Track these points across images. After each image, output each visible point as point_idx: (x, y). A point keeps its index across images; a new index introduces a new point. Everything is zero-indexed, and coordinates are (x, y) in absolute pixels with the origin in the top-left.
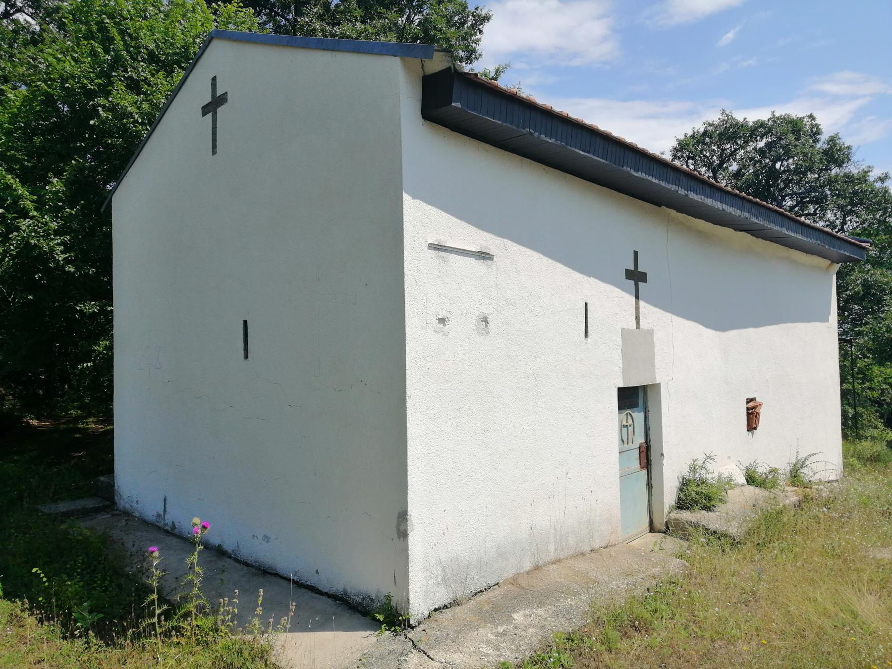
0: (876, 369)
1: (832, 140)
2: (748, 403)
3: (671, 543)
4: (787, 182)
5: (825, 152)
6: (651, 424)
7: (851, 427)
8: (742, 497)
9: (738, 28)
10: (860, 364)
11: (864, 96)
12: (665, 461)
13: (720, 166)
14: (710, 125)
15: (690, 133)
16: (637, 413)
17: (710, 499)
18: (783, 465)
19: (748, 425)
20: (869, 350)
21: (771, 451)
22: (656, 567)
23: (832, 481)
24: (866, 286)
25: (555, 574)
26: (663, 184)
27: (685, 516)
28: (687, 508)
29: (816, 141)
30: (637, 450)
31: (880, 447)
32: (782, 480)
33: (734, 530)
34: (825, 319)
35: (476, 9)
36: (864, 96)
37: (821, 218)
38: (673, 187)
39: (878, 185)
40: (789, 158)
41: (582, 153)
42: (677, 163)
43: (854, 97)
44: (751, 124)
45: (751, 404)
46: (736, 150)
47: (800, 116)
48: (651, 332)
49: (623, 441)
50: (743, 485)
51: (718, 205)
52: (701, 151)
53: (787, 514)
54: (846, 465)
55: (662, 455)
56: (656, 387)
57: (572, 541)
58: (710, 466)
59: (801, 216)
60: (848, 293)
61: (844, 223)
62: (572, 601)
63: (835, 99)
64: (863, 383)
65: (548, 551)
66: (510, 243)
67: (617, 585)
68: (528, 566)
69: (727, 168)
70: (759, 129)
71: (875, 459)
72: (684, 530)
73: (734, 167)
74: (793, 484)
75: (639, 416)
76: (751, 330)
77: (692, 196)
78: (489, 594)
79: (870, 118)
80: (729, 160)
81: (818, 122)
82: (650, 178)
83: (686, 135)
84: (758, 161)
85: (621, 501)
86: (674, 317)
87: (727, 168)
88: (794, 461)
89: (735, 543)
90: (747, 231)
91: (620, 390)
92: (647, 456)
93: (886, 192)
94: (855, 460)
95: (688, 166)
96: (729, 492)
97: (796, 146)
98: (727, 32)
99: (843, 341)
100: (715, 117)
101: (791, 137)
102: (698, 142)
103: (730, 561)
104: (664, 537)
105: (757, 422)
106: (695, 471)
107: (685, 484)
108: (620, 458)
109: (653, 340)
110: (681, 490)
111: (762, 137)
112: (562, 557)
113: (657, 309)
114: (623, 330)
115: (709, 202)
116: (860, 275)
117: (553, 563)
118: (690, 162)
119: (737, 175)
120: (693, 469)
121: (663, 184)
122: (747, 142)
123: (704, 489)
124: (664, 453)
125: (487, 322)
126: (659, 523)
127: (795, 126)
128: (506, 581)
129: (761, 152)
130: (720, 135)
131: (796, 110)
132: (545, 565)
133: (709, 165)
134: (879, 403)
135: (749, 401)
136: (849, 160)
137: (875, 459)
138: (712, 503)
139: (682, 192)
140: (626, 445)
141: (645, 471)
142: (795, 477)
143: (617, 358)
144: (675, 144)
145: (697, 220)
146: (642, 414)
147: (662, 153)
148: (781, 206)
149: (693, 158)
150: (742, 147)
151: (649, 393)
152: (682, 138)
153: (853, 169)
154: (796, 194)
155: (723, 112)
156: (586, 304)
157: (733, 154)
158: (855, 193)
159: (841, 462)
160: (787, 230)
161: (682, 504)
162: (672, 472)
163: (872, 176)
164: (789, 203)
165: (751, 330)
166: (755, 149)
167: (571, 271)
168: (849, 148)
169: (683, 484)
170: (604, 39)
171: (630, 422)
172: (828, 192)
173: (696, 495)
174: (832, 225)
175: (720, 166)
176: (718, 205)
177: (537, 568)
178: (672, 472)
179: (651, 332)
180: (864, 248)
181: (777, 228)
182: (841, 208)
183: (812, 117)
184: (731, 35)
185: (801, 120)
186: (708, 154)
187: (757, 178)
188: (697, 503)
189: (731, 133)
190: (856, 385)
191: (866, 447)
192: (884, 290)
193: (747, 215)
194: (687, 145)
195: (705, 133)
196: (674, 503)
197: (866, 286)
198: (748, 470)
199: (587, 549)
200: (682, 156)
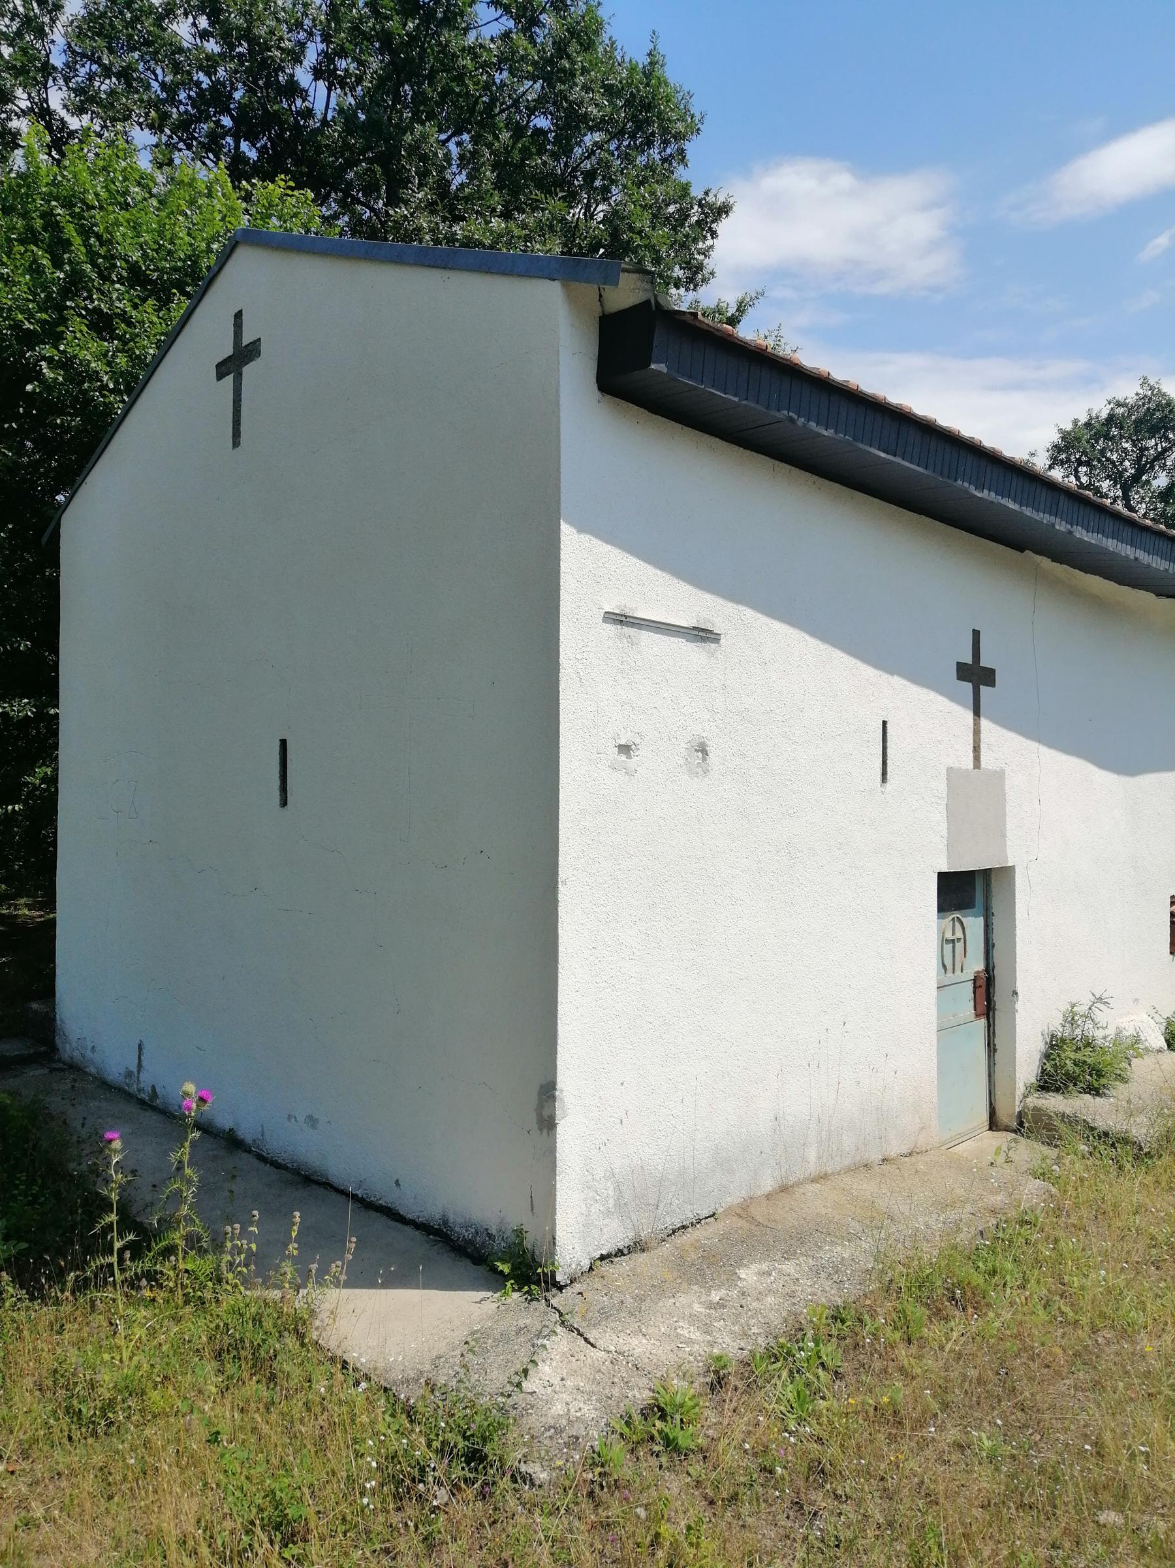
3: (1028, 1151)
6: (997, 938)
12: (1019, 1005)
13: (1136, 478)
14: (1119, 404)
15: (1083, 419)
22: (997, 1193)
25: (816, 1202)
26: (1028, 512)
27: (1054, 1103)
28: (1057, 1090)
30: (970, 985)
33: (1140, 1130)
35: (706, 193)
38: (1046, 518)
41: (883, 455)
42: (1057, 474)
49: (944, 966)
50: (1160, 1051)
51: (1127, 551)
55: (1015, 993)
58: (1099, 1016)
66: (749, 614)
68: (768, 1184)
69: (1148, 482)
72: (1050, 1128)
75: (974, 924)
77: (1080, 533)
78: (698, 1233)
80: (1152, 467)
82: (1004, 501)
83: (1075, 422)
86: (1043, 749)
87: (1148, 482)
89: (1141, 1155)
91: (942, 876)
92: (988, 995)
96: (1134, 1061)
100: (1129, 391)
106: (1073, 1022)
107: (1055, 1046)
108: (938, 998)
110: (1047, 1056)
112: (829, 1171)
114: (950, 770)
115: (1111, 544)
117: (814, 1181)
120: (1071, 1019)
124: (1019, 990)
126: (1004, 1116)
128: (729, 1211)
130: (1138, 422)
132: (799, 1184)
138: (1103, 1081)
139: (1061, 526)
140: (950, 974)
141: (983, 1022)
143: (938, 819)
144: (1056, 438)
151: (994, 884)
161: (1047, 1083)
167: (859, 663)
169: (1052, 1047)
171: (959, 934)
173: (1075, 1066)
175: (1136, 478)
176: (1127, 551)
177: (784, 1189)
179: (1000, 776)
186: (1114, 457)
194: (1078, 439)
199: (875, 1157)
200: (1068, 460)
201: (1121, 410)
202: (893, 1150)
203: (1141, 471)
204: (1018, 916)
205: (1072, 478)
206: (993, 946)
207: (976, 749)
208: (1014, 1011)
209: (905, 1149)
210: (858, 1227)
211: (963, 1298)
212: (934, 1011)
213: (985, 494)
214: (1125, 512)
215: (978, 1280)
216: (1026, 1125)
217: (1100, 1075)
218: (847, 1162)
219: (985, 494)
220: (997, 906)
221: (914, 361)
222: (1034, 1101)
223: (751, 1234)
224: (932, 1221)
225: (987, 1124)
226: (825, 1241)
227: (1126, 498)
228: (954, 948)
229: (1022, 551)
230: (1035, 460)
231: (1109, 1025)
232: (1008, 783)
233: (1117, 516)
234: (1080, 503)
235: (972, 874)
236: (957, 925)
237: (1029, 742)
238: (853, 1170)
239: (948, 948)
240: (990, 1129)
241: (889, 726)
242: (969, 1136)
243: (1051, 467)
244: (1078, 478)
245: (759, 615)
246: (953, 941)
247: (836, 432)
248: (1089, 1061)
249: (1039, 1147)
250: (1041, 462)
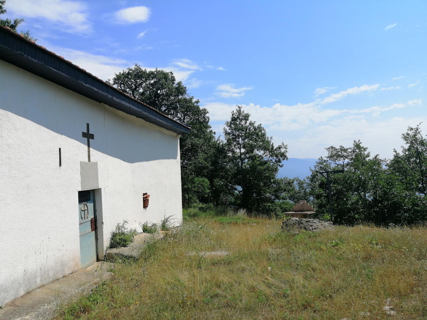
0: (196, 179)
1: (179, 84)
2: (143, 195)
3: (106, 265)
4: (163, 100)
5: (177, 88)
6: (97, 208)
7: (186, 203)
8: (141, 238)
9: (145, 32)
10: (191, 177)
11: (192, 70)
12: (104, 226)
13: (135, 89)
14: (130, 70)
15: (122, 73)
16: (89, 204)
17: (125, 241)
18: (159, 222)
19: (144, 205)
20: (193, 171)
21: (153, 216)
22: (97, 278)
23: (178, 226)
24: (192, 145)
25: (39, 294)
26: (100, 92)
27: (114, 251)
28: (115, 247)
29: (173, 83)
30: (90, 222)
31: (196, 210)
32: (159, 229)
33: (135, 253)
34: (175, 158)
36: (192, 70)
37: (176, 116)
38: (105, 94)
39: (196, 104)
40: (163, 89)
41: (55, 70)
42: (115, 86)
43: (189, 70)
44: (148, 72)
45: (145, 196)
46: (142, 83)
47: (167, 72)
48: (96, 164)
49: (82, 218)
50: (141, 233)
51: (128, 105)
52: (127, 82)
53: (160, 243)
54: (184, 219)
55: (103, 223)
56: (99, 190)
57: (51, 274)
58: (126, 226)
59: (168, 114)
60: (186, 148)
61: (184, 119)
62: (47, 307)
63: (183, 69)
64: (192, 185)
65: (36, 282)
66: (10, 114)
67: (73, 292)
68: (22, 292)
69: (138, 90)
70: (151, 75)
71: (195, 215)
72: (113, 258)
73: (141, 90)
74: (163, 230)
75: (90, 205)
76: (145, 163)
77: (115, 99)
79: (195, 79)
80: (139, 87)
81: (174, 75)
82: (93, 88)
83: (120, 73)
84: (151, 89)
85: (81, 250)
86: (108, 156)
87: (138, 90)
88: (163, 219)
89: (136, 260)
90: (142, 118)
91: (80, 192)
92: (96, 224)
93: (198, 107)
94: (188, 216)
95: (121, 88)
96: (135, 237)
97: (166, 84)
98: (141, 33)
99: (182, 167)
100: (133, 67)
101: (164, 80)
102: (126, 77)
103: (133, 270)
104: (103, 263)
105: (148, 204)
106: (119, 229)
107: (114, 235)
108: (80, 227)
109: (97, 167)
110: (112, 239)
111: (152, 79)
112: (45, 283)
113: (99, 152)
114: (81, 162)
115: (123, 102)
116: (190, 141)
117: (39, 288)
118: (122, 85)
119: (143, 94)
120: (118, 228)
121: (100, 92)
122: (146, 80)
123: (122, 237)
124: (104, 222)
126: (101, 257)
127: (165, 76)
128: (7, 305)
129: (152, 85)
130: (135, 75)
131: (166, 70)
132: (34, 290)
133: (131, 88)
134: (198, 192)
135: (144, 194)
136: (185, 93)
137: (195, 215)
138: (127, 243)
139: (110, 96)
140: (83, 220)
141: (94, 232)
142: (164, 227)
143: (78, 176)
144: (115, 76)
145: (119, 111)
146: (92, 204)
147: (109, 80)
148: (160, 109)
149: (123, 84)
150: (144, 82)
151: (96, 194)
152: (118, 74)
153: (187, 97)
154: (166, 105)
155: (136, 65)
156: (60, 149)
157: (141, 84)
158: (188, 107)
159: (182, 218)
160: (159, 118)
161: (112, 246)
162: (107, 231)
163: (194, 100)
164: (163, 109)
165: (145, 163)
166: (150, 83)
167: (51, 131)
168: (185, 88)
169: (113, 236)
170: (84, 23)
171: (86, 208)
172: (178, 105)
173: (120, 240)
174: (180, 119)
175: (135, 89)
176: (128, 105)
177: (28, 293)
178: (107, 231)
179: (96, 164)
180: (189, 129)
181: (154, 117)
182: (182, 112)
183: (171, 73)
184: (142, 34)
185: (168, 73)
186: (130, 83)
187: (151, 96)
188: (119, 244)
189: (139, 75)
190: (189, 185)
191: (192, 210)
192: (198, 147)
193: (141, 110)
194: (121, 77)
195: (129, 73)
196: (108, 246)
197: (192, 145)
198: (144, 226)
199: (61, 276)
200: (118, 83)
201: (131, 71)
202: (67, 272)
203: (136, 87)
204: (103, 202)
205: (119, 87)
207: (89, 156)
209: (70, 272)
210: (53, 298)
211: (85, 310)
212: (78, 231)
213: (88, 85)
214: (133, 98)
215: (89, 303)
216: (109, 258)
217: (126, 241)
218: (51, 279)
219: (88, 85)
220: (97, 200)
221: (80, 53)
222: (109, 251)
223: (15, 310)
224: (77, 291)
225: (96, 260)
226: (41, 306)
227: (133, 94)
230: (110, 81)
231: (128, 228)
232: (99, 166)
233: (132, 99)
234: (120, 94)
236: (85, 206)
237: (104, 154)
238: (53, 282)
239: (83, 212)
240: (97, 261)
242: (91, 264)
243: (114, 84)
244: (121, 88)
245: (14, 115)
246: (84, 210)
247: (38, 61)
248: (123, 238)
249: (109, 263)
250: (112, 82)
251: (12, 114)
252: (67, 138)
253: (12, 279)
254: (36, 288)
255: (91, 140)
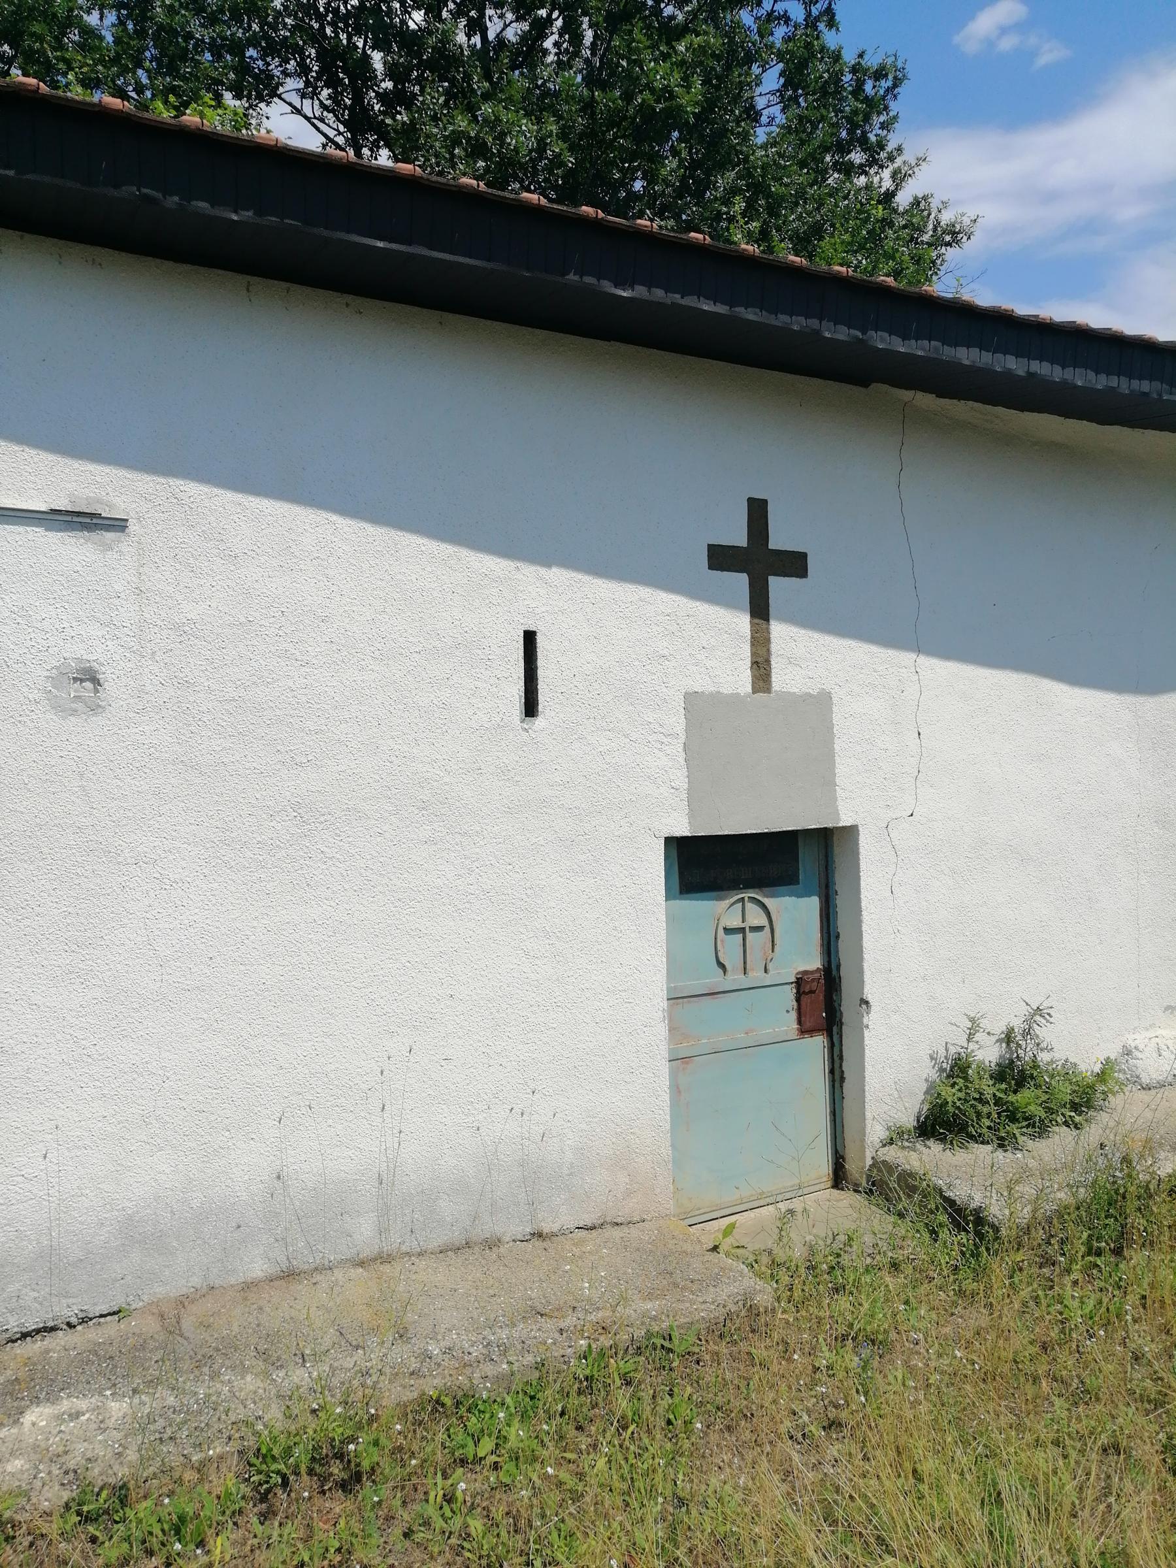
6: (842, 923)
16: (788, 901)
30: (790, 993)
35: (861, 56)
41: (380, 244)
51: (1013, 364)
58: (1043, 1032)
66: (192, 490)
78: (61, 1338)
82: (690, 301)
92: (826, 1003)
112: (545, 1231)
114: (691, 699)
124: (870, 998)
125: (96, 681)
126: (852, 1167)
132: (562, 1233)
141: (818, 1043)
146: (814, 903)
151: (837, 850)
156: (530, 638)
161: (939, 1124)
167: (464, 552)
171: (762, 921)
176: (1013, 364)
177: (290, 1275)
206: (838, 937)
208: (861, 1028)
216: (884, 1186)
222: (891, 1154)
228: (744, 939)
229: (866, 386)
235: (793, 835)
241: (540, 640)
245: (216, 490)
251: (205, 489)
252: (586, 578)
253: (195, 1204)
254: (342, 1263)
255: (778, 585)
